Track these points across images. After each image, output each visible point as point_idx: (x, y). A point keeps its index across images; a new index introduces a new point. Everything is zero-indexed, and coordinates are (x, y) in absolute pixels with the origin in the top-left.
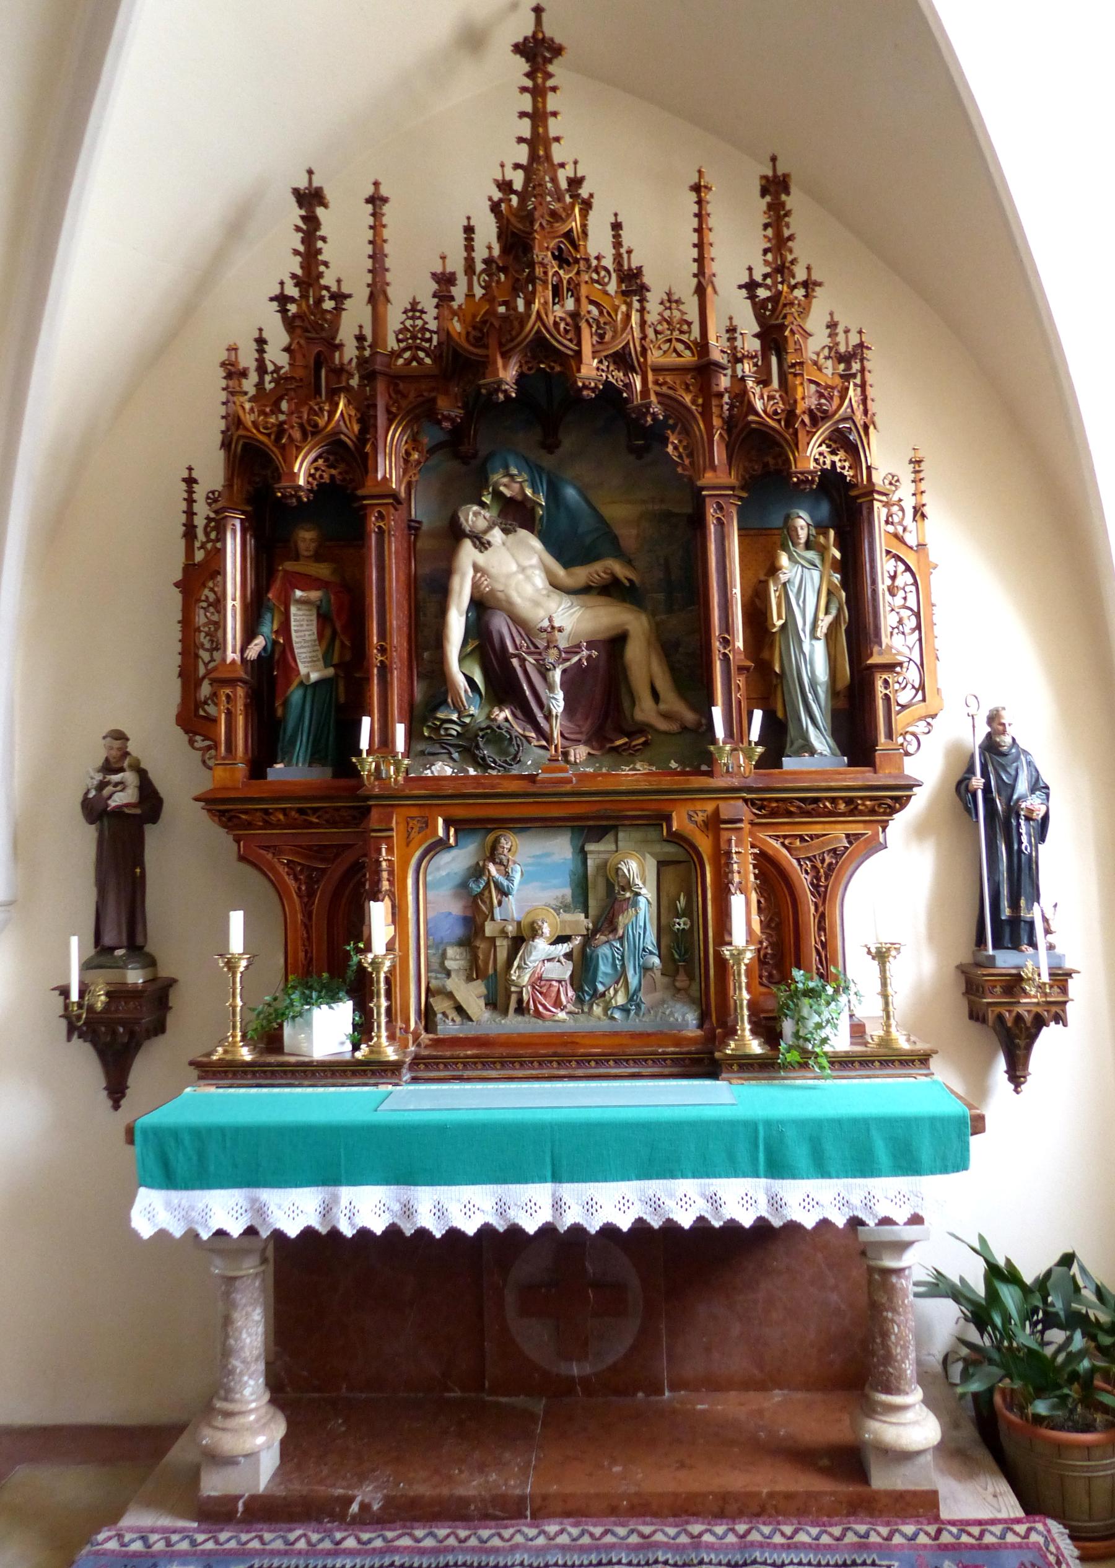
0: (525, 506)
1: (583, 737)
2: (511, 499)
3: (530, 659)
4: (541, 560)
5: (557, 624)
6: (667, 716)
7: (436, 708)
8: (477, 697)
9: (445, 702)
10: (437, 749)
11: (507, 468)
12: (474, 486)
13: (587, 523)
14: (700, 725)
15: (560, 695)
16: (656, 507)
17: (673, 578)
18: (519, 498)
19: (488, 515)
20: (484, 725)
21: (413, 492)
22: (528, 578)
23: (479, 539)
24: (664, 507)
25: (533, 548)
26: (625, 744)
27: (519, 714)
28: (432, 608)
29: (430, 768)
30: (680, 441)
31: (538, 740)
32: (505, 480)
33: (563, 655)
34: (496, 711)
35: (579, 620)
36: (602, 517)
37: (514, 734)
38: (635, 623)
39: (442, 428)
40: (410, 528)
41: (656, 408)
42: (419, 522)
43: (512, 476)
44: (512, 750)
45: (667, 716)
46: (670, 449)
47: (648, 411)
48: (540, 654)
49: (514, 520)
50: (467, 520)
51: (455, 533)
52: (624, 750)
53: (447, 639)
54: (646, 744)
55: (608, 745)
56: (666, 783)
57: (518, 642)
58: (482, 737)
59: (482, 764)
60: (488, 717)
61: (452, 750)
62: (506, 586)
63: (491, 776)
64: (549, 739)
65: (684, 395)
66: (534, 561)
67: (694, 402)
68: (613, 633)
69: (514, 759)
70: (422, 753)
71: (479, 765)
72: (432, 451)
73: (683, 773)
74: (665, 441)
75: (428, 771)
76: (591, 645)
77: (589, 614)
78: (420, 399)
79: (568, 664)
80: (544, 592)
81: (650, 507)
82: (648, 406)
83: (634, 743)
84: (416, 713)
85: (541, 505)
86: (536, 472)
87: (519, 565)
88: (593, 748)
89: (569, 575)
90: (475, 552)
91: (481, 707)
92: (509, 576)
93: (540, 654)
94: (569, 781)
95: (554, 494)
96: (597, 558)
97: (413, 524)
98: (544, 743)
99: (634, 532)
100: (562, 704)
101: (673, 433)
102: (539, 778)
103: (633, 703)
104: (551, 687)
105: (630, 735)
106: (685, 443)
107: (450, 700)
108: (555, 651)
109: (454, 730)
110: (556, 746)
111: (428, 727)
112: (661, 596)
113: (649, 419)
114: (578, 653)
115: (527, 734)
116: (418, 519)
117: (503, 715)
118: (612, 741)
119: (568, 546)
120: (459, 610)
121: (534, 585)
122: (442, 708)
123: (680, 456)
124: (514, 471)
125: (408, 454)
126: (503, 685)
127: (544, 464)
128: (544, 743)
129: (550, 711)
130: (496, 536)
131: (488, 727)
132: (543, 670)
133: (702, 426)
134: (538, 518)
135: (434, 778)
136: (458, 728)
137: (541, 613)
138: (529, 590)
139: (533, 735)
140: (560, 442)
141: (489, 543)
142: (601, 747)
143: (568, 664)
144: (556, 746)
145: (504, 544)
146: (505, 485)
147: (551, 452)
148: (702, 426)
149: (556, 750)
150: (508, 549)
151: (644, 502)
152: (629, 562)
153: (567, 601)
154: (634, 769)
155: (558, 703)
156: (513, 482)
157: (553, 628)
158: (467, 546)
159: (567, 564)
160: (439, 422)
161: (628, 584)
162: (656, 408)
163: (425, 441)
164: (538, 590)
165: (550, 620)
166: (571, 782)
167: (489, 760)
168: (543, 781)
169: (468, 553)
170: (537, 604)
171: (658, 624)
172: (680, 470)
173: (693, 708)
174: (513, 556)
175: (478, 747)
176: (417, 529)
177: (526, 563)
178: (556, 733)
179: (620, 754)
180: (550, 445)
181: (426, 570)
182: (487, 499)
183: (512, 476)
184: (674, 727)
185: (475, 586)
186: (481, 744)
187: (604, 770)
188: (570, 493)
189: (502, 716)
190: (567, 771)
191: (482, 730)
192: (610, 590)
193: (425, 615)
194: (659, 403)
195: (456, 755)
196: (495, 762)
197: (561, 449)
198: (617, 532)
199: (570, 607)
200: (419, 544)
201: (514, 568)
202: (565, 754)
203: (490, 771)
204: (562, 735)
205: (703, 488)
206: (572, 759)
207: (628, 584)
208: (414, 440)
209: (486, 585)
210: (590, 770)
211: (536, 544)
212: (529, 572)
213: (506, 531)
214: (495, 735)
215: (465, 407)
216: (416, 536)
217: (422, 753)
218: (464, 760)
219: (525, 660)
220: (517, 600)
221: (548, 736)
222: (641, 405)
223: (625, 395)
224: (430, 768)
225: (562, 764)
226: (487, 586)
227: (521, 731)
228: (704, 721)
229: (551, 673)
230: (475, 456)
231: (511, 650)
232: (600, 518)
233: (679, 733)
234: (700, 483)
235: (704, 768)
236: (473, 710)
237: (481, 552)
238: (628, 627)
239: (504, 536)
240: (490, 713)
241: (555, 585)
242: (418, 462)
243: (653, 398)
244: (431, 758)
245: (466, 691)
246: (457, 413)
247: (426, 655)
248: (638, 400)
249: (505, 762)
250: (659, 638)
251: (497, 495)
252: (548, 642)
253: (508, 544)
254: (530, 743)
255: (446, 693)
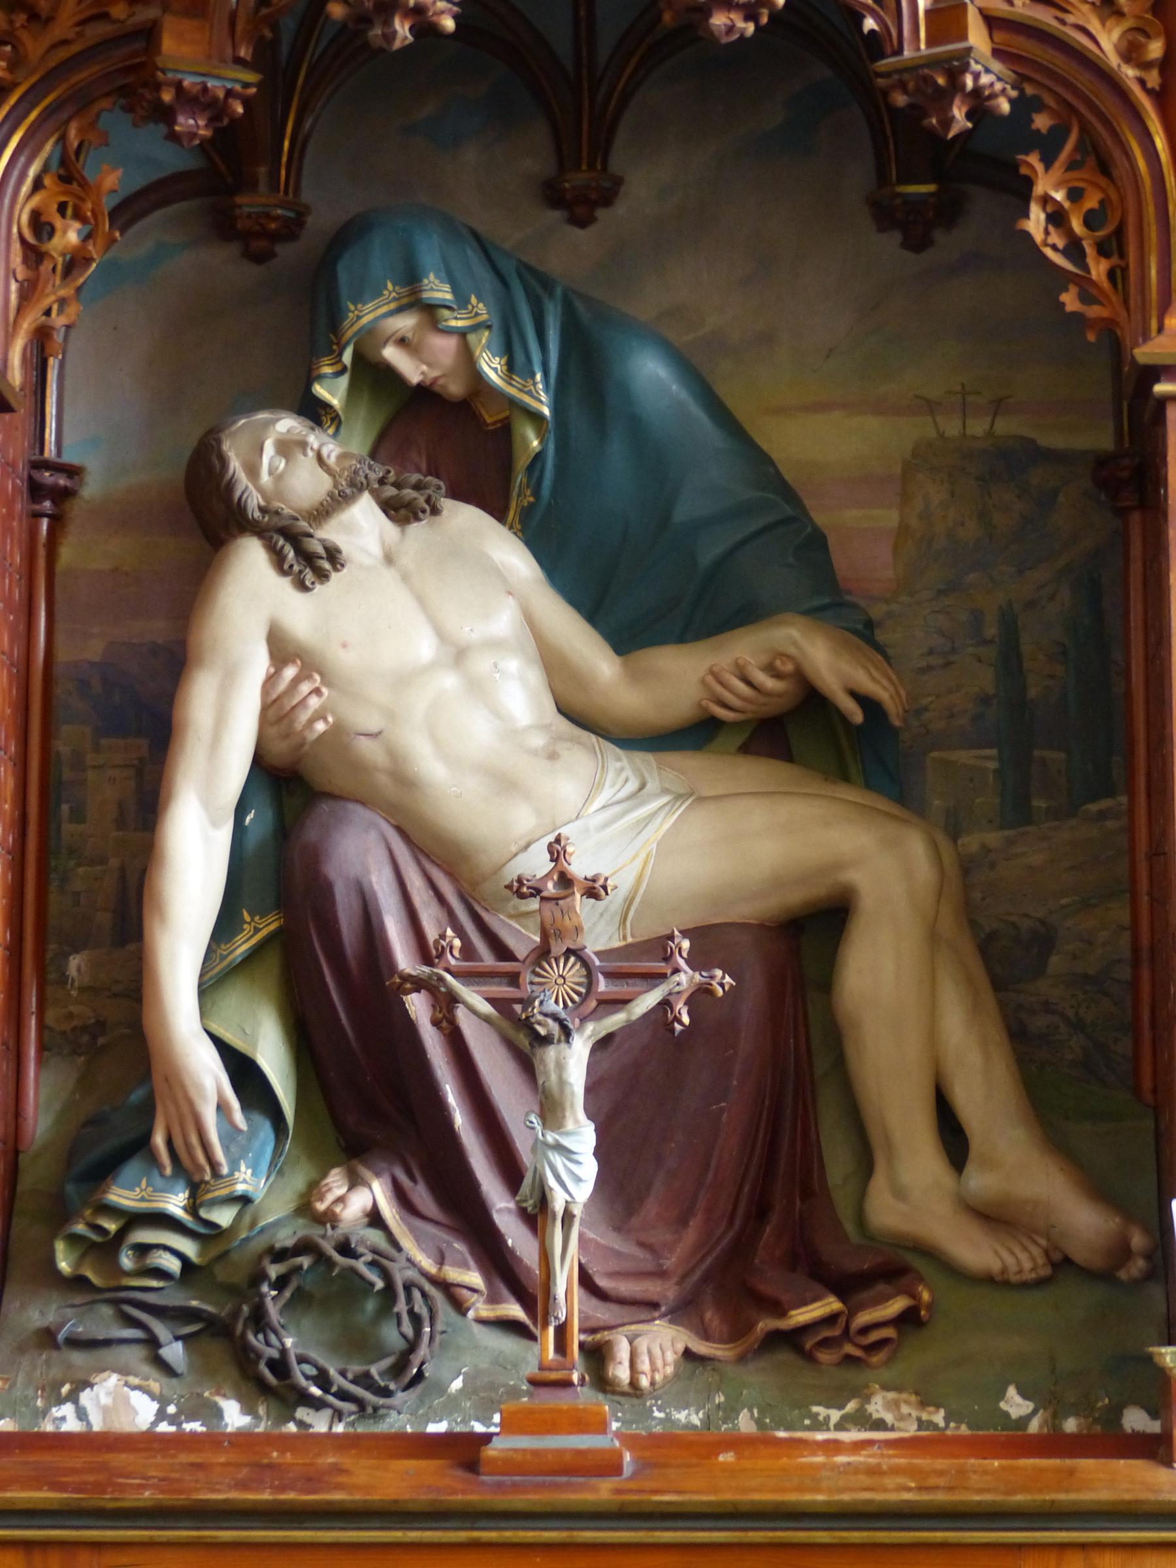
0: (476, 418)
1: (666, 1291)
2: (424, 393)
3: (474, 997)
4: (529, 619)
5: (580, 867)
6: (993, 1217)
7: (105, 1170)
8: (266, 1130)
9: (141, 1145)
10: (102, 1322)
11: (411, 278)
12: (288, 334)
13: (708, 483)
14: (1122, 1252)
15: (582, 1135)
16: (978, 427)
17: (1033, 692)
18: (455, 388)
19: (332, 450)
20: (285, 1238)
21: (53, 363)
22: (477, 689)
23: (295, 538)
24: (1006, 426)
25: (497, 573)
26: (830, 1320)
27: (421, 1195)
28: (104, 790)
29: (73, 1397)
30: (1075, 195)
31: (493, 1299)
32: (406, 323)
33: (602, 985)
34: (336, 1183)
35: (664, 847)
36: (769, 461)
37: (400, 1276)
38: (885, 863)
39: (173, 137)
40: (36, 491)
41: (987, 73)
42: (73, 472)
43: (430, 311)
44: (392, 1336)
45: (993, 1217)
46: (1035, 222)
47: (955, 84)
48: (513, 979)
49: (433, 471)
50: (253, 471)
51: (207, 516)
52: (825, 1343)
53: (160, 909)
54: (909, 1320)
55: (765, 1324)
56: (986, 1479)
57: (431, 934)
58: (280, 1284)
59: (274, 1386)
60: (304, 1209)
61: (161, 1330)
62: (390, 715)
63: (307, 1440)
64: (533, 1295)
65: (1094, 26)
66: (504, 621)
67: (1131, 52)
68: (795, 898)
69: (398, 1369)
70: (47, 1338)
71: (264, 1389)
72: (129, 210)
73: (1053, 1444)
74: (1020, 191)
75: (67, 1409)
76: (709, 943)
77: (703, 826)
78: (99, 30)
79: (616, 1020)
80: (538, 741)
81: (952, 427)
82: (956, 67)
83: (864, 1318)
84: (26, 1182)
85: (535, 417)
86: (521, 292)
87: (441, 635)
88: (706, 1335)
89: (635, 676)
90: (283, 586)
91: (277, 1168)
92: (404, 680)
93: (513, 979)
94: (609, 1466)
95: (587, 374)
96: (746, 614)
97: (47, 477)
98: (515, 1311)
99: (890, 518)
100: (589, 1168)
101: (1048, 163)
102: (493, 1450)
103: (865, 1164)
104: (550, 1109)
105: (847, 1286)
106: (1092, 202)
107: (159, 1140)
108: (573, 972)
109: (174, 1250)
110: (562, 1332)
111: (74, 1240)
112: (987, 760)
113: (959, 112)
114: (656, 978)
115: (453, 1274)
116: (68, 458)
117: (360, 1199)
118: (779, 1309)
119: (632, 569)
120: (207, 803)
121: (497, 713)
122: (132, 1169)
123: (1074, 250)
124: (438, 291)
125: (40, 225)
126: (364, 1080)
127: (555, 264)
128: (515, 1311)
129: (544, 1201)
130: (362, 527)
131: (305, 1247)
132: (523, 1041)
133: (1160, 143)
134: (522, 462)
135: (87, 1442)
136: (188, 1247)
137: (522, 819)
138: (478, 732)
139: (475, 1278)
140: (618, 182)
141: (334, 555)
142: (736, 1331)
143: (616, 1020)
144: (562, 1332)
145: (389, 559)
146: (402, 342)
147: (582, 222)
148: (1160, 143)
149: (561, 1345)
150: (405, 578)
151: (931, 407)
152: (864, 633)
153: (622, 771)
154: (862, 1420)
155: (574, 1167)
156: (432, 330)
157: (565, 881)
158: (250, 562)
159: (625, 639)
160: (166, 115)
161: (857, 716)
162: (987, 73)
163: (111, 180)
164: (511, 734)
165: (557, 851)
166: (614, 1468)
167: (300, 1374)
168: (513, 1465)
169: (251, 592)
170: (506, 784)
171: (967, 867)
172: (1070, 300)
173: (1099, 1189)
174: (421, 601)
175: (259, 1320)
176: (62, 495)
177: (470, 630)
178: (564, 1279)
179: (809, 1357)
180: (578, 197)
181: (85, 648)
182: (332, 392)
183: (430, 311)
184: (1019, 1259)
185: (275, 714)
186: (273, 1311)
187: (745, 1423)
188: (650, 373)
189: (358, 1203)
190: (601, 1427)
191: (279, 1255)
192: (791, 732)
193: (78, 815)
194: (997, 53)
195: (174, 1352)
196: (323, 1380)
197: (621, 208)
198: (821, 519)
199: (638, 795)
200: (67, 554)
201: (425, 657)
202: (597, 1356)
203: (302, 1413)
204: (586, 1280)
205: (1155, 373)
206: (621, 1373)
207: (857, 716)
208: (67, 171)
209: (315, 713)
210: (689, 1417)
211: (512, 557)
212: (482, 664)
213: (399, 511)
214: (327, 1276)
215: (265, 58)
216: (58, 521)
217: (47, 1338)
218: (205, 1370)
219: (453, 999)
220: (431, 767)
221: (534, 1283)
222: (935, 62)
223: (870, 24)
224: (73, 1397)
225: (586, 1397)
226: (320, 715)
227: (427, 1263)
228: (1138, 1240)
229: (551, 1053)
230: (292, 229)
231: (404, 959)
232: (758, 461)
233: (1040, 1283)
234: (1145, 353)
235: (1135, 1420)
236: (246, 1180)
237: (302, 586)
238: (855, 877)
239: (390, 529)
240: (314, 1189)
241: (579, 714)
242: (75, 262)
243: (977, 37)
244: (77, 1358)
245: (222, 1108)
246: (231, 81)
247: (75, 964)
248: (917, 46)
249: (364, 1380)
250: (969, 913)
251: (373, 376)
252: (545, 935)
253: (406, 560)
254: (460, 1307)
255: (147, 1111)
